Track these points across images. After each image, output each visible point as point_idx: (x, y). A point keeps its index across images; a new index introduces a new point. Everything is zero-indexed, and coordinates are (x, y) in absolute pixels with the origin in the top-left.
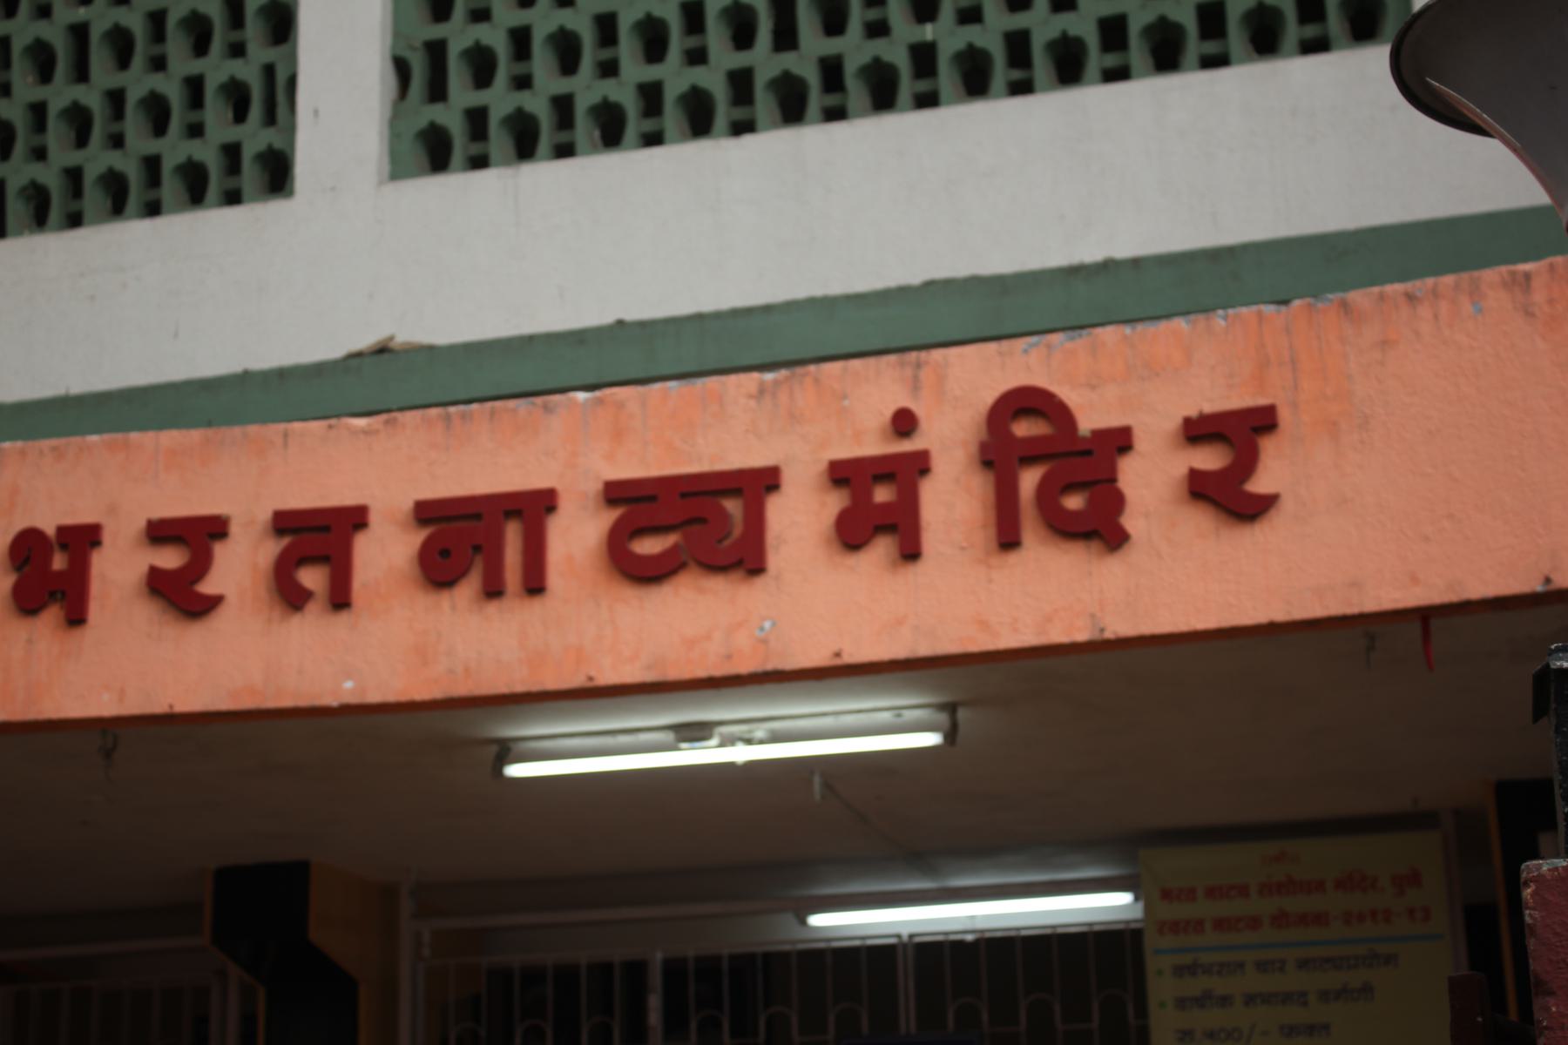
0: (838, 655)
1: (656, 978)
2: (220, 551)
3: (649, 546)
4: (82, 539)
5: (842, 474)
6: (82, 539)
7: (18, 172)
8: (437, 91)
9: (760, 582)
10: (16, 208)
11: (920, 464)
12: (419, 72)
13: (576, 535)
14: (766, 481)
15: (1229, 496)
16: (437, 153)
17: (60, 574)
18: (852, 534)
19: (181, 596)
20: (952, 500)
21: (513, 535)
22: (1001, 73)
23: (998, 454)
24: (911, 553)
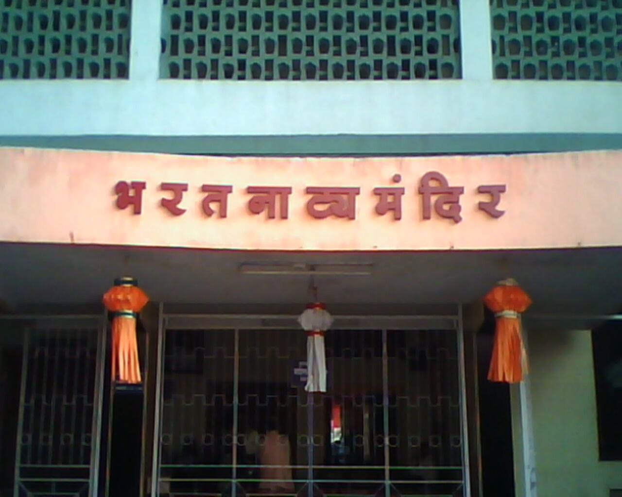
0: (579, 244)
1: (385, 335)
2: (185, 194)
3: (319, 208)
4: (140, 187)
5: (377, 192)
6: (140, 187)
7: (8, 59)
8: (174, 52)
9: (353, 222)
10: (7, 70)
11: (402, 191)
12: (169, 45)
13: (297, 203)
14: (357, 191)
15: (489, 210)
16: (173, 72)
17: (132, 197)
18: (379, 211)
19: (171, 208)
20: (410, 204)
21: (278, 198)
22: (182, 72)
23: (423, 190)
24: (398, 218)
